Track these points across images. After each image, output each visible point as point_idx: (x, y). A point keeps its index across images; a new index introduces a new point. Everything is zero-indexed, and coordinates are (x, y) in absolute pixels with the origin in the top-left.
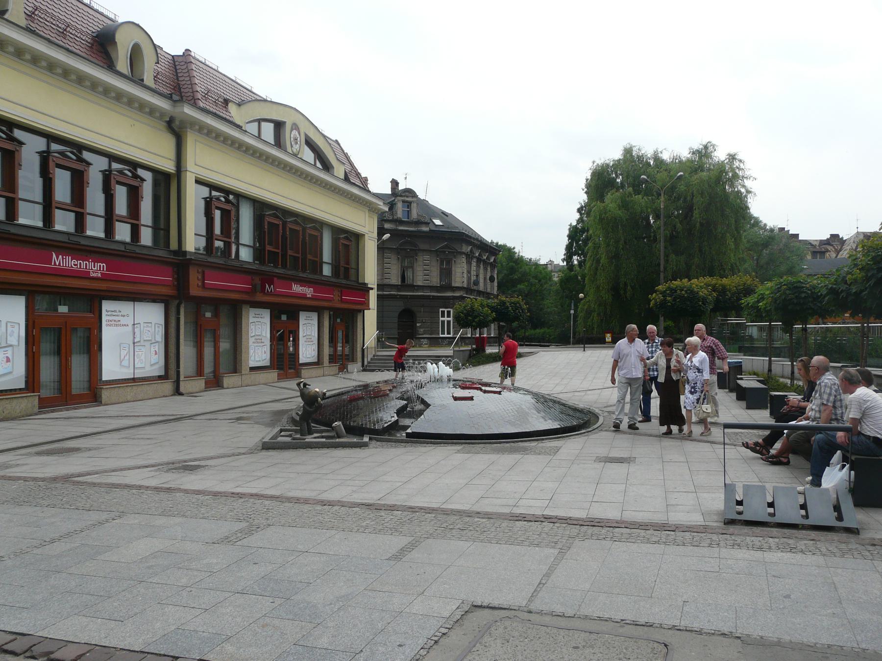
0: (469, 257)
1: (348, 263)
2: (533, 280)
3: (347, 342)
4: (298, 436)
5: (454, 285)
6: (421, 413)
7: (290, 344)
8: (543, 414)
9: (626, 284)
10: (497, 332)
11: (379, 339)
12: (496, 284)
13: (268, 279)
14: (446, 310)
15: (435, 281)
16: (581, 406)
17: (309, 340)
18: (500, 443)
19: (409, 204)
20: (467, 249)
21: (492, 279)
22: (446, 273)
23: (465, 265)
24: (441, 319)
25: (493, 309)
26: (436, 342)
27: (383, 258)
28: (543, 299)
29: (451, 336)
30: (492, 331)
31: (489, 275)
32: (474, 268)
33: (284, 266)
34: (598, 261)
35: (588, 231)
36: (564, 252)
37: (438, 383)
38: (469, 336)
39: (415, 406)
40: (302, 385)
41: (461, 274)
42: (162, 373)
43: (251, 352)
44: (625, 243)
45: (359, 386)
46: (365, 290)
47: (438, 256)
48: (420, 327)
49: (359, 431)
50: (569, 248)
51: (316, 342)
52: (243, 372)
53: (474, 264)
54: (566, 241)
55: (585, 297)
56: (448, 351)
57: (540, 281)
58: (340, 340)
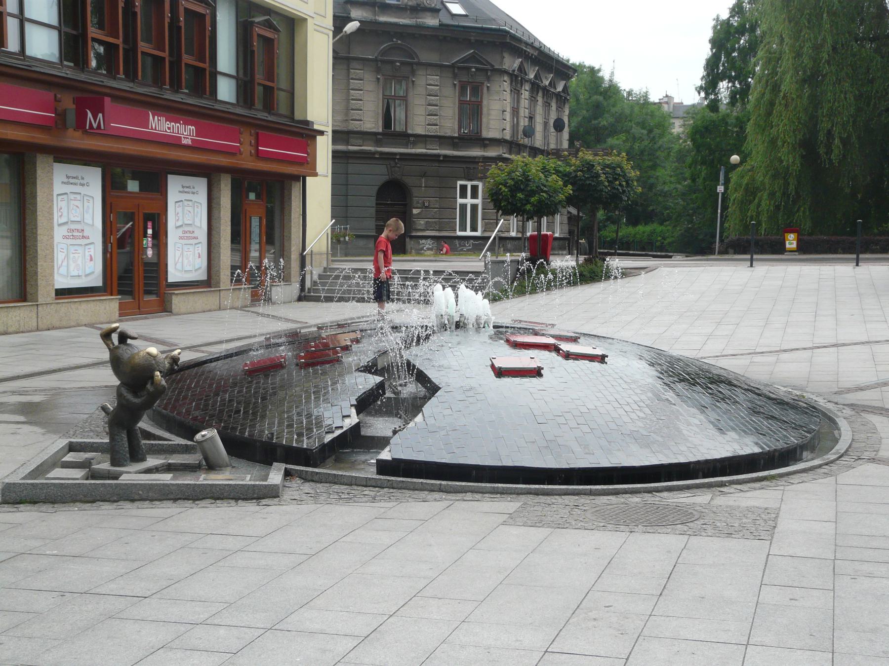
0: (517, 79)
1: (270, 74)
2: (637, 131)
3: (270, 240)
4: (105, 466)
5: (486, 134)
6: (415, 406)
7: (148, 242)
8: (713, 416)
9: (829, 133)
10: (566, 228)
11: (337, 240)
12: (566, 134)
13: (90, 100)
14: (469, 184)
15: (449, 126)
16: (781, 391)
17: (188, 235)
18: (616, 493)
20: (512, 63)
21: (559, 126)
22: (472, 111)
23: (507, 96)
24: (460, 201)
25: (568, 178)
26: (450, 244)
27: (348, 78)
28: (654, 167)
29: (478, 234)
30: (556, 227)
31: (553, 116)
32: (524, 103)
33: (131, 75)
34: (776, 88)
35: (753, 29)
36: (701, 72)
38: (513, 234)
39: (399, 390)
40: (115, 337)
41: (500, 111)
42: (202, 275)
43: (59, 256)
44: (834, 49)
45: (278, 335)
46: (306, 134)
47: (455, 76)
48: (419, 216)
49: (264, 453)
50: (712, 65)
51: (204, 239)
52: (41, 300)
53: (525, 94)
54: (705, 51)
55: (742, 162)
56: (474, 263)
57: (650, 131)
58: (255, 237)
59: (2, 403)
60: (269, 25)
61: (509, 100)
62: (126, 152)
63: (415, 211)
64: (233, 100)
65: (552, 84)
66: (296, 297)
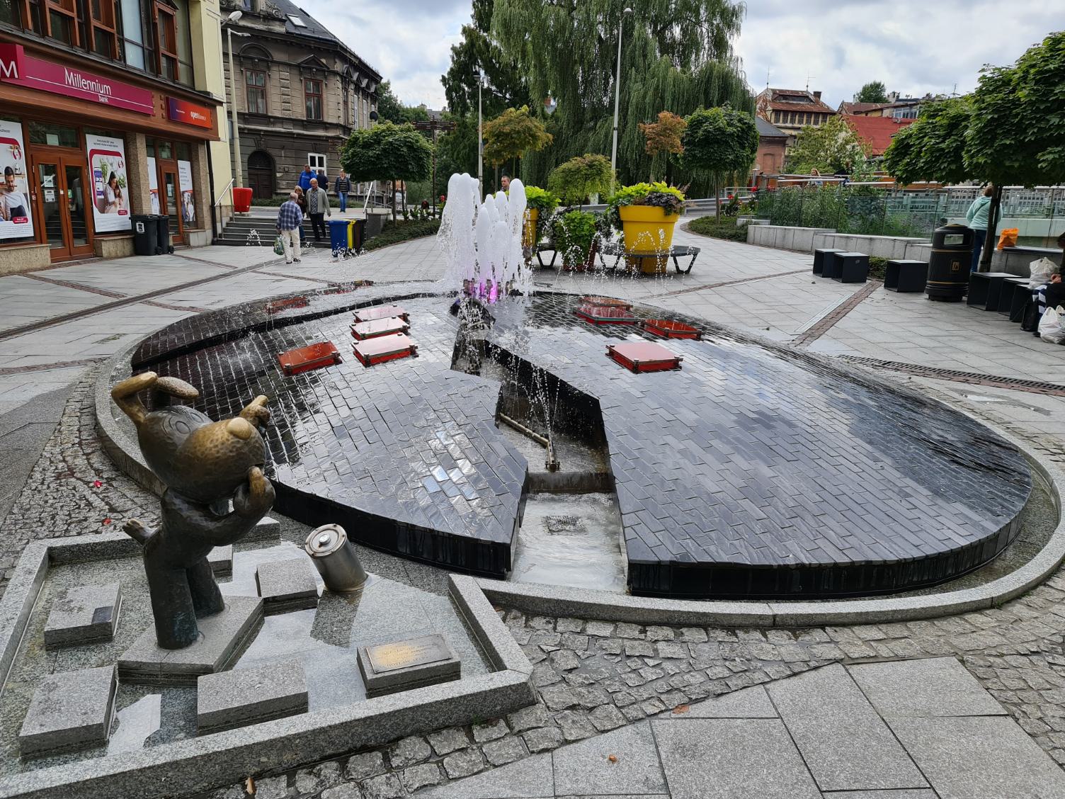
0: (345, 79)
1: (172, 47)
14: (317, 156)
15: (299, 112)
20: (339, 67)
23: (340, 92)
37: (761, 229)
47: (301, 74)
61: (341, 94)
63: (278, 175)
65: (368, 86)
66: (209, 241)
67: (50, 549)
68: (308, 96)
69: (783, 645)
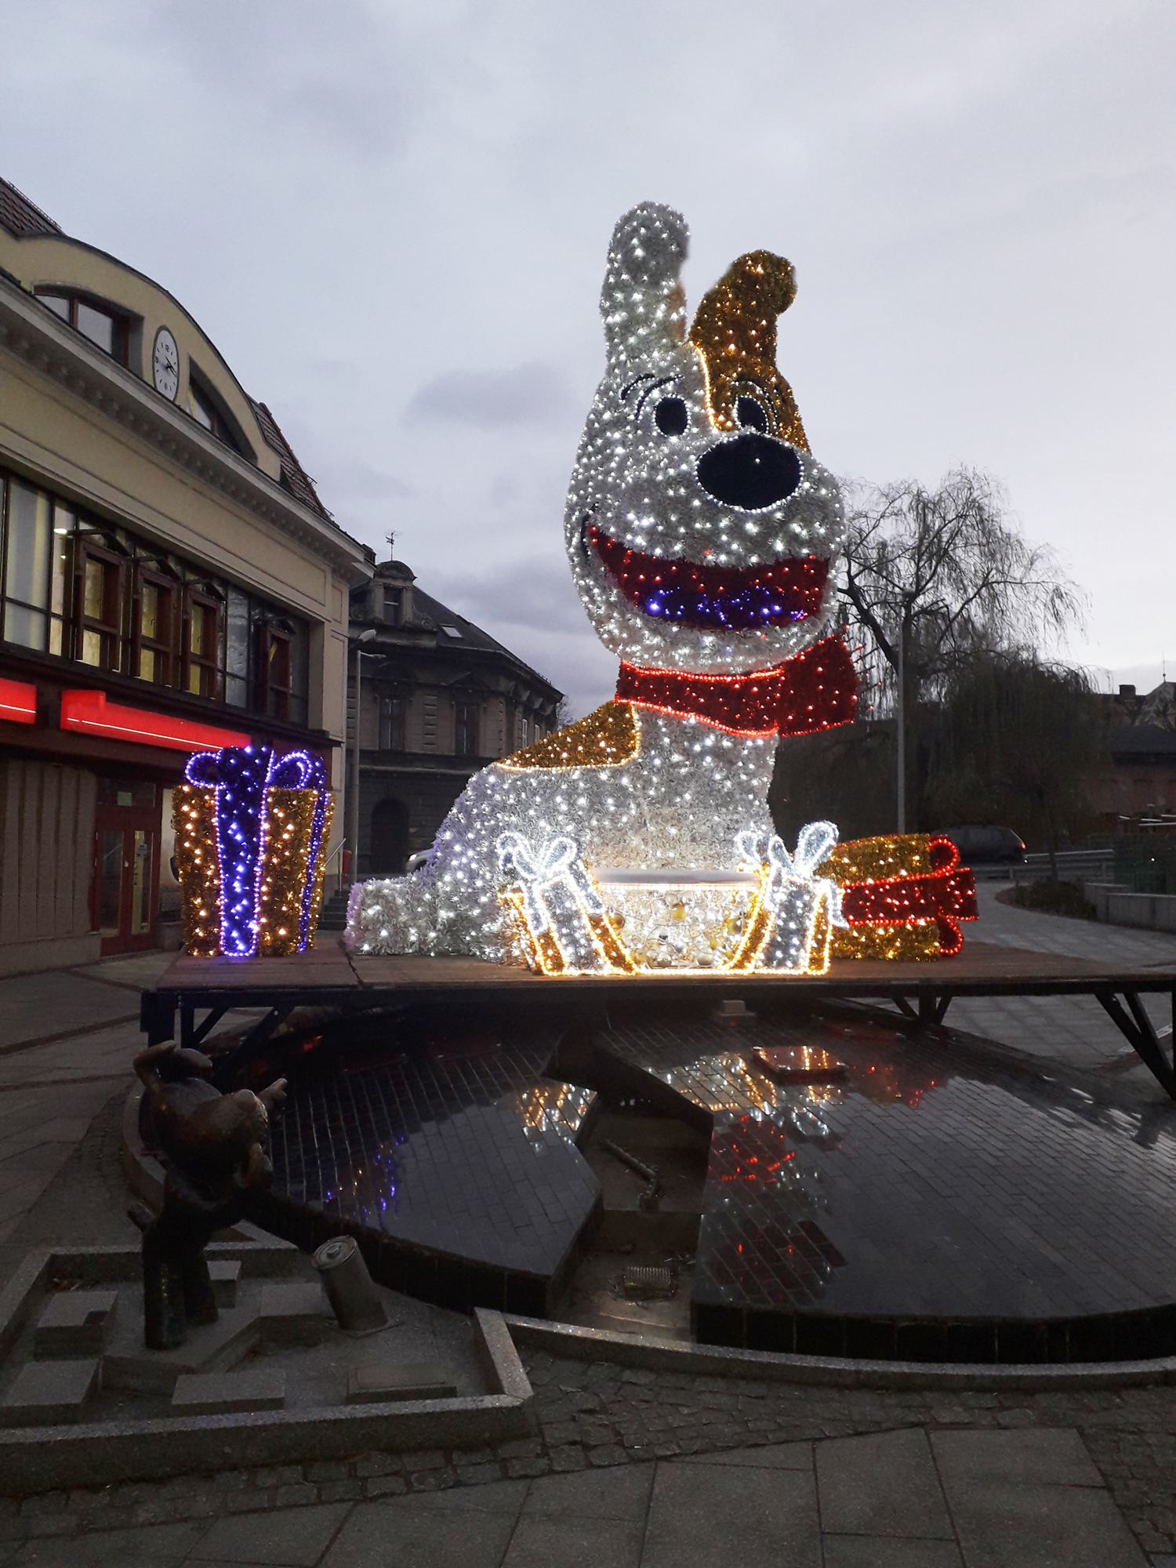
0: (512, 702)
16: (1084, 924)
19: (395, 594)
20: (505, 685)
23: (503, 716)
59: (4, 1446)
60: (284, 626)
62: (1132, 1363)
63: (412, 830)
64: (242, 705)
65: (542, 707)
67: (54, 1257)
68: (459, 722)
69: (866, 1406)
